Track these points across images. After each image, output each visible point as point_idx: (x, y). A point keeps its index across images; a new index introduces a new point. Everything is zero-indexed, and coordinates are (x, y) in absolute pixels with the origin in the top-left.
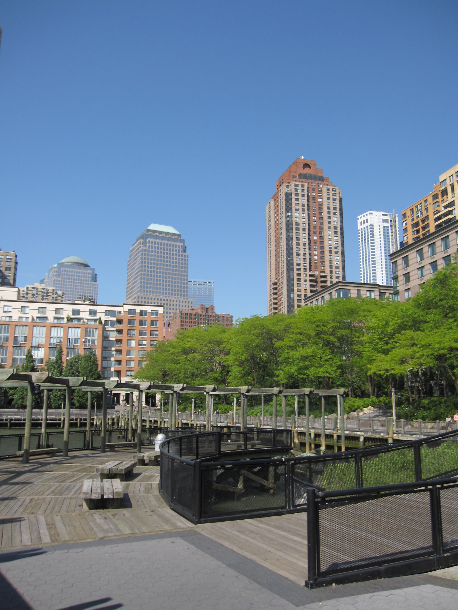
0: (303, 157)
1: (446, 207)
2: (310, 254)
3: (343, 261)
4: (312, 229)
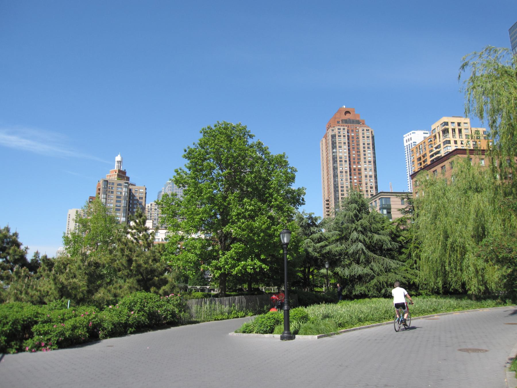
0: (344, 107)
1: (436, 148)
2: (351, 179)
3: (376, 182)
4: (352, 160)
